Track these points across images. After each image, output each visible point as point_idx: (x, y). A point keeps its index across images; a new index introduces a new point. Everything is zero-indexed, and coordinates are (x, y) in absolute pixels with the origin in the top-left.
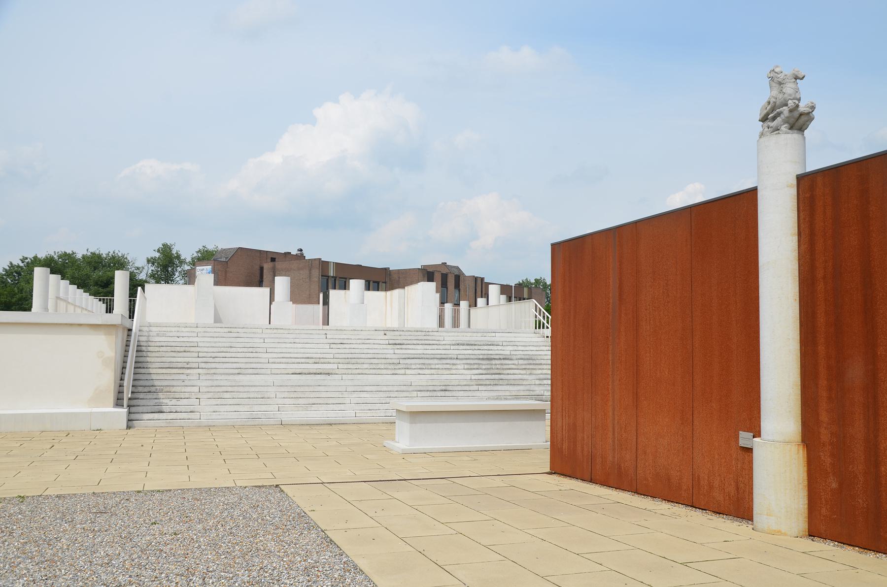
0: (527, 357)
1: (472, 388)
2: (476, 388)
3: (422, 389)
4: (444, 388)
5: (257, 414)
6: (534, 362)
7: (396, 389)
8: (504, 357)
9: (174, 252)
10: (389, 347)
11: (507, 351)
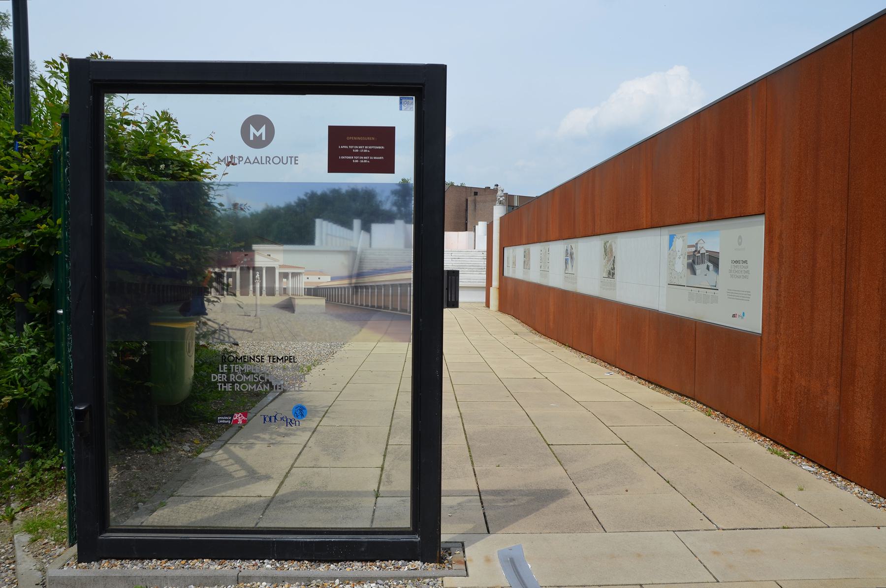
7: (478, 281)
10: (482, 260)
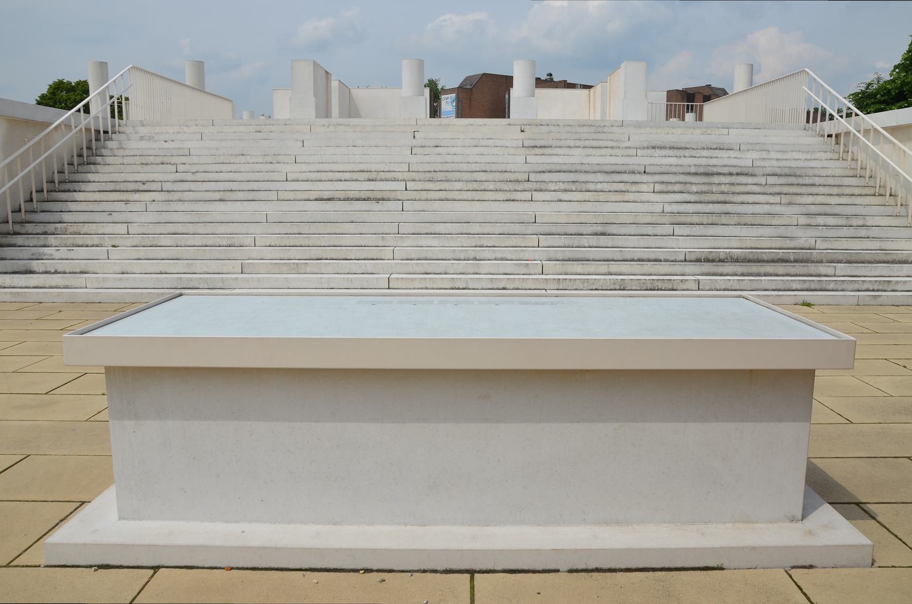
0: (787, 171)
1: (659, 230)
2: (668, 229)
3: (553, 229)
4: (599, 229)
5: (191, 279)
6: (800, 181)
7: (499, 229)
8: (739, 170)
9: (440, 87)
11: (746, 160)
